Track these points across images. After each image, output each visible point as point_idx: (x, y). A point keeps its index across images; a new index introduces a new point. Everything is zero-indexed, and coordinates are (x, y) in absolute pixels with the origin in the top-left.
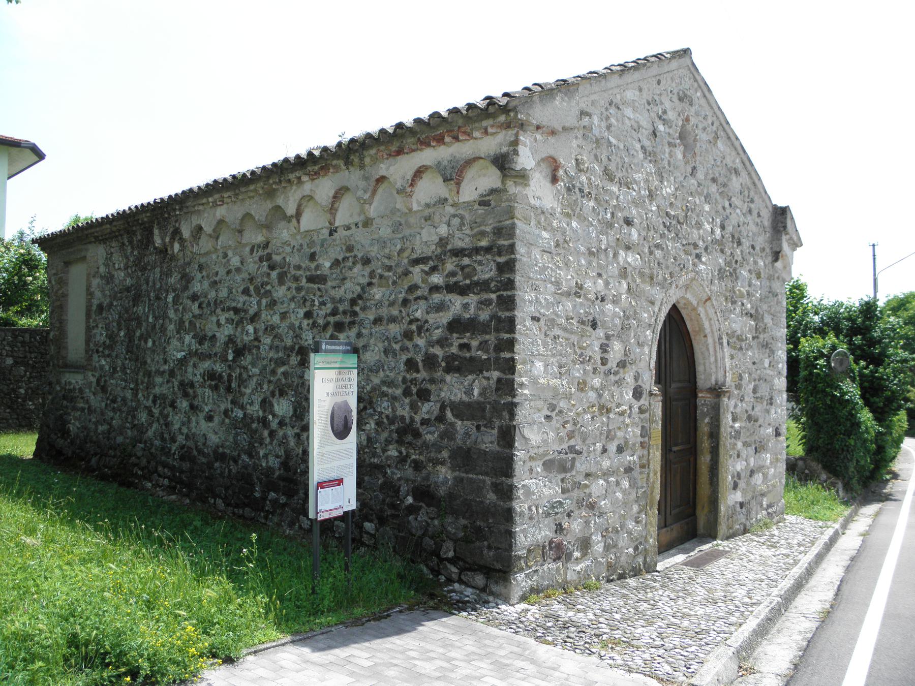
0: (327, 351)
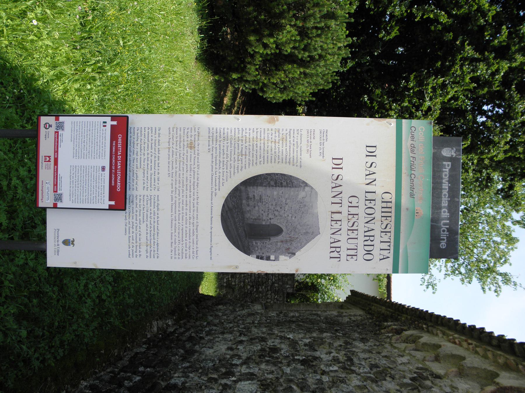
0: (437, 161)
